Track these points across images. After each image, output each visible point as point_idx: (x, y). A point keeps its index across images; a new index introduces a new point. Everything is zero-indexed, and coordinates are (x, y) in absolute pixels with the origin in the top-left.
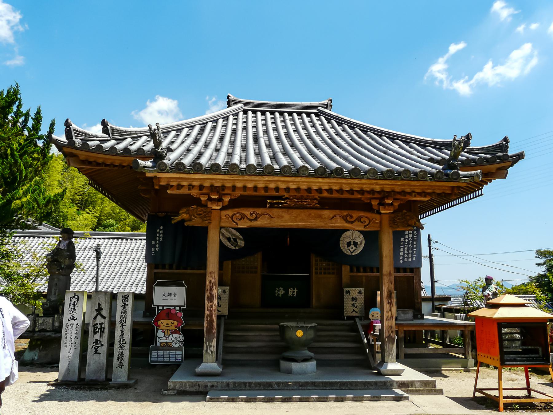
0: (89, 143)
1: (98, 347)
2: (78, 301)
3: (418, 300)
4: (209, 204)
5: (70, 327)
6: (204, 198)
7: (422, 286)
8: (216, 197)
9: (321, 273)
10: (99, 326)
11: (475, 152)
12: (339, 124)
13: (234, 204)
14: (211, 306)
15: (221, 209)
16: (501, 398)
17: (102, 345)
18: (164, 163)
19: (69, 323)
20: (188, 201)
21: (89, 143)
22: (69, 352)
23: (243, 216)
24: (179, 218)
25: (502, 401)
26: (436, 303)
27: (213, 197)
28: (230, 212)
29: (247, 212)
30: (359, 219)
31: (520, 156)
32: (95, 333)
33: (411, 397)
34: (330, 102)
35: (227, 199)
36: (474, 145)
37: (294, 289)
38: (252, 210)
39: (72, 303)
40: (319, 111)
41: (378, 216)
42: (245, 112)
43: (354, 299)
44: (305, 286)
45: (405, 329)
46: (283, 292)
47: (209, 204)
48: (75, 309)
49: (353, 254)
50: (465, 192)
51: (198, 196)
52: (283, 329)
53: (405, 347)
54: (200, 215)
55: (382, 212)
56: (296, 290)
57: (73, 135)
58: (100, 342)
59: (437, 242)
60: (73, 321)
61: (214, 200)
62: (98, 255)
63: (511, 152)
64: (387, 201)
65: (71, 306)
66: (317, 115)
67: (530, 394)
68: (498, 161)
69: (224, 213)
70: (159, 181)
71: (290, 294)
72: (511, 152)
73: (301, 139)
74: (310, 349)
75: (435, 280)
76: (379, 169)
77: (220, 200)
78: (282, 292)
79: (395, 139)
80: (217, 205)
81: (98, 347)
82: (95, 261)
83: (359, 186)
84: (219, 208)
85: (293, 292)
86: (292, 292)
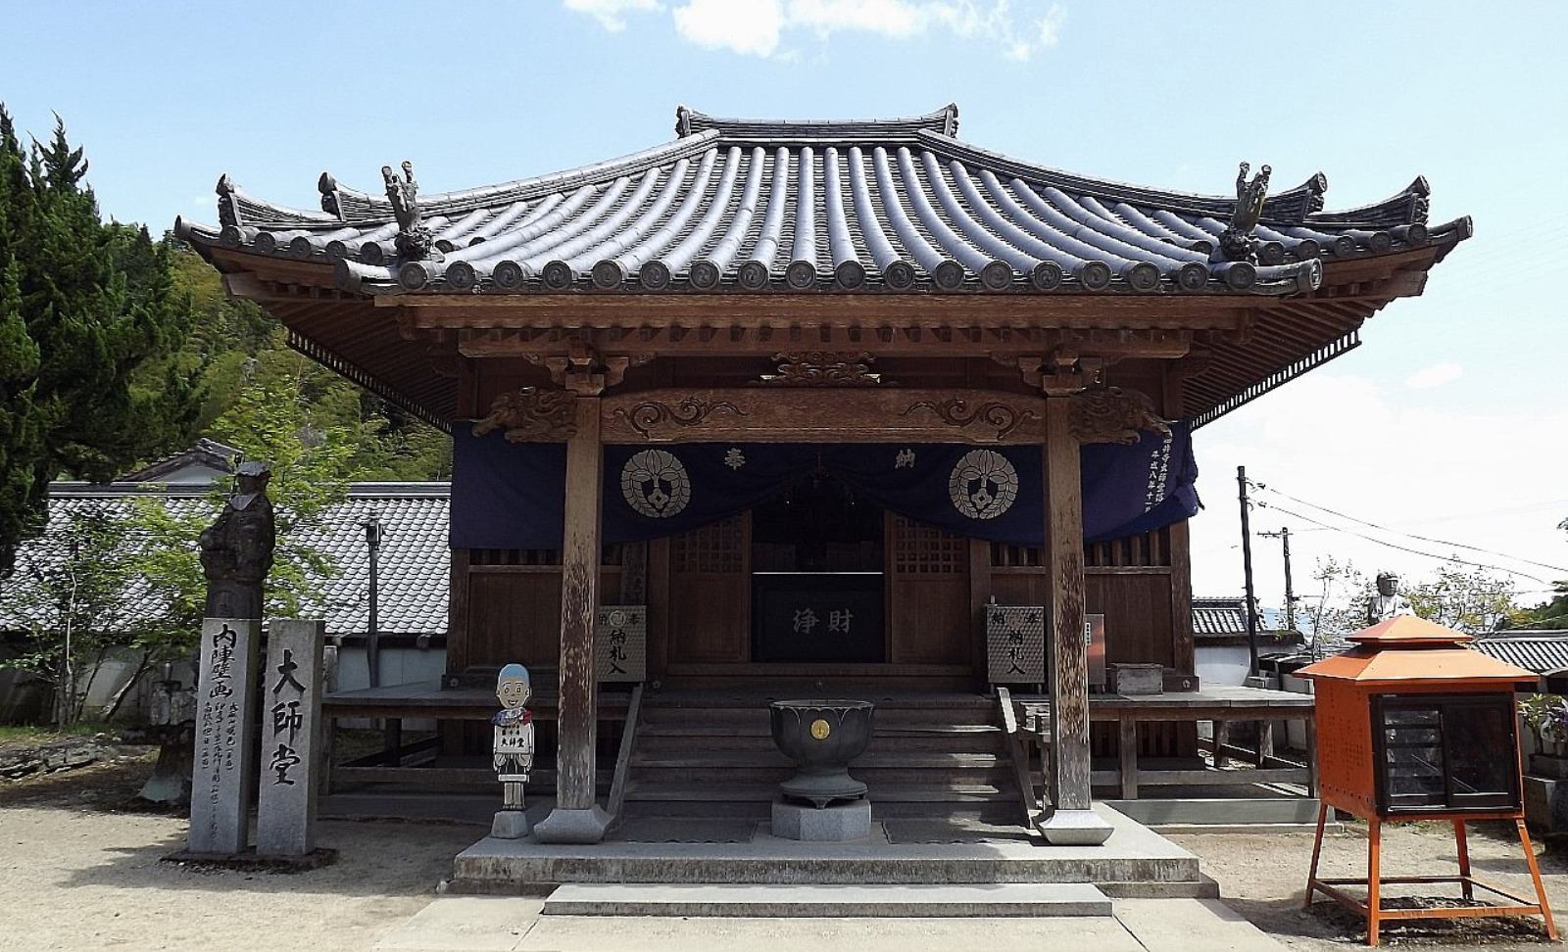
0: (274, 234)
1: (287, 765)
2: (233, 645)
3: (1182, 639)
4: (570, 382)
5: (214, 713)
6: (556, 367)
7: (1257, 611)
11: (1328, 223)
12: (974, 171)
13: (639, 380)
14: (577, 656)
15: (602, 395)
16: (1375, 904)
17: (297, 760)
18: (419, 267)
20: (513, 374)
21: (274, 234)
22: (214, 778)
23: (663, 413)
24: (490, 422)
25: (1377, 916)
26: (1262, 653)
27: (577, 362)
28: (626, 402)
29: (673, 400)
30: (982, 413)
31: (1460, 230)
32: (278, 729)
33: (1119, 905)
34: (950, 113)
35: (619, 368)
38: (684, 395)
39: (220, 649)
40: (924, 139)
41: (1038, 402)
42: (724, 149)
43: (1016, 637)
44: (871, 600)
45: (1140, 719)
46: (815, 620)
47: (570, 382)
48: (225, 667)
49: (982, 517)
50: (1314, 341)
51: (541, 362)
52: (779, 718)
53: (1140, 767)
54: (544, 411)
55: (1049, 391)
56: (848, 616)
57: (236, 212)
58: (292, 752)
61: (582, 369)
62: (372, 533)
63: (1436, 218)
64: (1062, 362)
65: (218, 661)
66: (916, 151)
67: (1470, 895)
68: (1398, 247)
69: (611, 403)
70: (415, 320)
71: (833, 627)
72: (1436, 218)
74: (854, 773)
75: (1294, 595)
76: (1018, 264)
77: (600, 369)
79: (1117, 202)
80: (592, 385)
81: (287, 765)
82: (366, 549)
83: (965, 315)
85: (842, 621)
86: (840, 621)
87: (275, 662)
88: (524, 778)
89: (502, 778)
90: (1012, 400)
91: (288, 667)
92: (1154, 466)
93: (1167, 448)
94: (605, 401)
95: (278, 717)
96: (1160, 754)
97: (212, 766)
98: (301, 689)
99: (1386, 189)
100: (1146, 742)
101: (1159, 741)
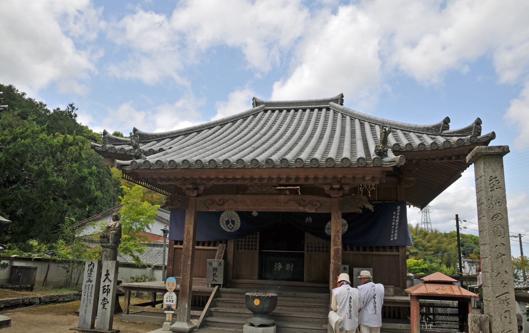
6: (327, 188)
8: (338, 186)
9: (312, 251)
10: (106, 288)
13: (208, 192)
15: (196, 196)
19: (87, 284)
23: (213, 202)
29: (217, 198)
32: (104, 293)
35: (202, 188)
36: (453, 127)
37: (291, 265)
38: (220, 196)
46: (281, 267)
48: (91, 274)
54: (180, 201)
56: (292, 266)
59: (465, 221)
60: (89, 283)
61: (336, 189)
69: (198, 198)
73: (303, 133)
78: (280, 267)
84: (195, 195)
85: (290, 267)
87: (104, 273)
88: (173, 312)
89: (166, 312)
90: (321, 199)
91: (107, 275)
92: (394, 217)
93: (399, 211)
94: (197, 198)
95: (104, 289)
96: (394, 317)
97: (86, 303)
98: (111, 281)
99: (469, 122)
100: (195, 301)
101: (199, 302)
